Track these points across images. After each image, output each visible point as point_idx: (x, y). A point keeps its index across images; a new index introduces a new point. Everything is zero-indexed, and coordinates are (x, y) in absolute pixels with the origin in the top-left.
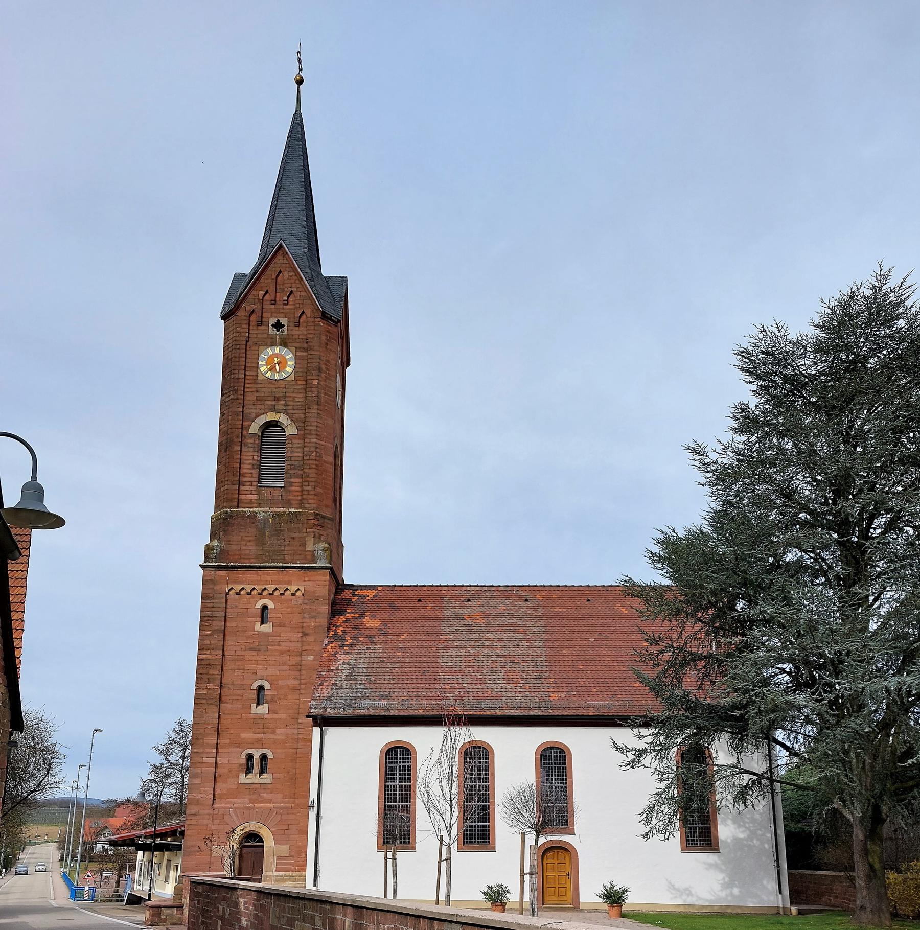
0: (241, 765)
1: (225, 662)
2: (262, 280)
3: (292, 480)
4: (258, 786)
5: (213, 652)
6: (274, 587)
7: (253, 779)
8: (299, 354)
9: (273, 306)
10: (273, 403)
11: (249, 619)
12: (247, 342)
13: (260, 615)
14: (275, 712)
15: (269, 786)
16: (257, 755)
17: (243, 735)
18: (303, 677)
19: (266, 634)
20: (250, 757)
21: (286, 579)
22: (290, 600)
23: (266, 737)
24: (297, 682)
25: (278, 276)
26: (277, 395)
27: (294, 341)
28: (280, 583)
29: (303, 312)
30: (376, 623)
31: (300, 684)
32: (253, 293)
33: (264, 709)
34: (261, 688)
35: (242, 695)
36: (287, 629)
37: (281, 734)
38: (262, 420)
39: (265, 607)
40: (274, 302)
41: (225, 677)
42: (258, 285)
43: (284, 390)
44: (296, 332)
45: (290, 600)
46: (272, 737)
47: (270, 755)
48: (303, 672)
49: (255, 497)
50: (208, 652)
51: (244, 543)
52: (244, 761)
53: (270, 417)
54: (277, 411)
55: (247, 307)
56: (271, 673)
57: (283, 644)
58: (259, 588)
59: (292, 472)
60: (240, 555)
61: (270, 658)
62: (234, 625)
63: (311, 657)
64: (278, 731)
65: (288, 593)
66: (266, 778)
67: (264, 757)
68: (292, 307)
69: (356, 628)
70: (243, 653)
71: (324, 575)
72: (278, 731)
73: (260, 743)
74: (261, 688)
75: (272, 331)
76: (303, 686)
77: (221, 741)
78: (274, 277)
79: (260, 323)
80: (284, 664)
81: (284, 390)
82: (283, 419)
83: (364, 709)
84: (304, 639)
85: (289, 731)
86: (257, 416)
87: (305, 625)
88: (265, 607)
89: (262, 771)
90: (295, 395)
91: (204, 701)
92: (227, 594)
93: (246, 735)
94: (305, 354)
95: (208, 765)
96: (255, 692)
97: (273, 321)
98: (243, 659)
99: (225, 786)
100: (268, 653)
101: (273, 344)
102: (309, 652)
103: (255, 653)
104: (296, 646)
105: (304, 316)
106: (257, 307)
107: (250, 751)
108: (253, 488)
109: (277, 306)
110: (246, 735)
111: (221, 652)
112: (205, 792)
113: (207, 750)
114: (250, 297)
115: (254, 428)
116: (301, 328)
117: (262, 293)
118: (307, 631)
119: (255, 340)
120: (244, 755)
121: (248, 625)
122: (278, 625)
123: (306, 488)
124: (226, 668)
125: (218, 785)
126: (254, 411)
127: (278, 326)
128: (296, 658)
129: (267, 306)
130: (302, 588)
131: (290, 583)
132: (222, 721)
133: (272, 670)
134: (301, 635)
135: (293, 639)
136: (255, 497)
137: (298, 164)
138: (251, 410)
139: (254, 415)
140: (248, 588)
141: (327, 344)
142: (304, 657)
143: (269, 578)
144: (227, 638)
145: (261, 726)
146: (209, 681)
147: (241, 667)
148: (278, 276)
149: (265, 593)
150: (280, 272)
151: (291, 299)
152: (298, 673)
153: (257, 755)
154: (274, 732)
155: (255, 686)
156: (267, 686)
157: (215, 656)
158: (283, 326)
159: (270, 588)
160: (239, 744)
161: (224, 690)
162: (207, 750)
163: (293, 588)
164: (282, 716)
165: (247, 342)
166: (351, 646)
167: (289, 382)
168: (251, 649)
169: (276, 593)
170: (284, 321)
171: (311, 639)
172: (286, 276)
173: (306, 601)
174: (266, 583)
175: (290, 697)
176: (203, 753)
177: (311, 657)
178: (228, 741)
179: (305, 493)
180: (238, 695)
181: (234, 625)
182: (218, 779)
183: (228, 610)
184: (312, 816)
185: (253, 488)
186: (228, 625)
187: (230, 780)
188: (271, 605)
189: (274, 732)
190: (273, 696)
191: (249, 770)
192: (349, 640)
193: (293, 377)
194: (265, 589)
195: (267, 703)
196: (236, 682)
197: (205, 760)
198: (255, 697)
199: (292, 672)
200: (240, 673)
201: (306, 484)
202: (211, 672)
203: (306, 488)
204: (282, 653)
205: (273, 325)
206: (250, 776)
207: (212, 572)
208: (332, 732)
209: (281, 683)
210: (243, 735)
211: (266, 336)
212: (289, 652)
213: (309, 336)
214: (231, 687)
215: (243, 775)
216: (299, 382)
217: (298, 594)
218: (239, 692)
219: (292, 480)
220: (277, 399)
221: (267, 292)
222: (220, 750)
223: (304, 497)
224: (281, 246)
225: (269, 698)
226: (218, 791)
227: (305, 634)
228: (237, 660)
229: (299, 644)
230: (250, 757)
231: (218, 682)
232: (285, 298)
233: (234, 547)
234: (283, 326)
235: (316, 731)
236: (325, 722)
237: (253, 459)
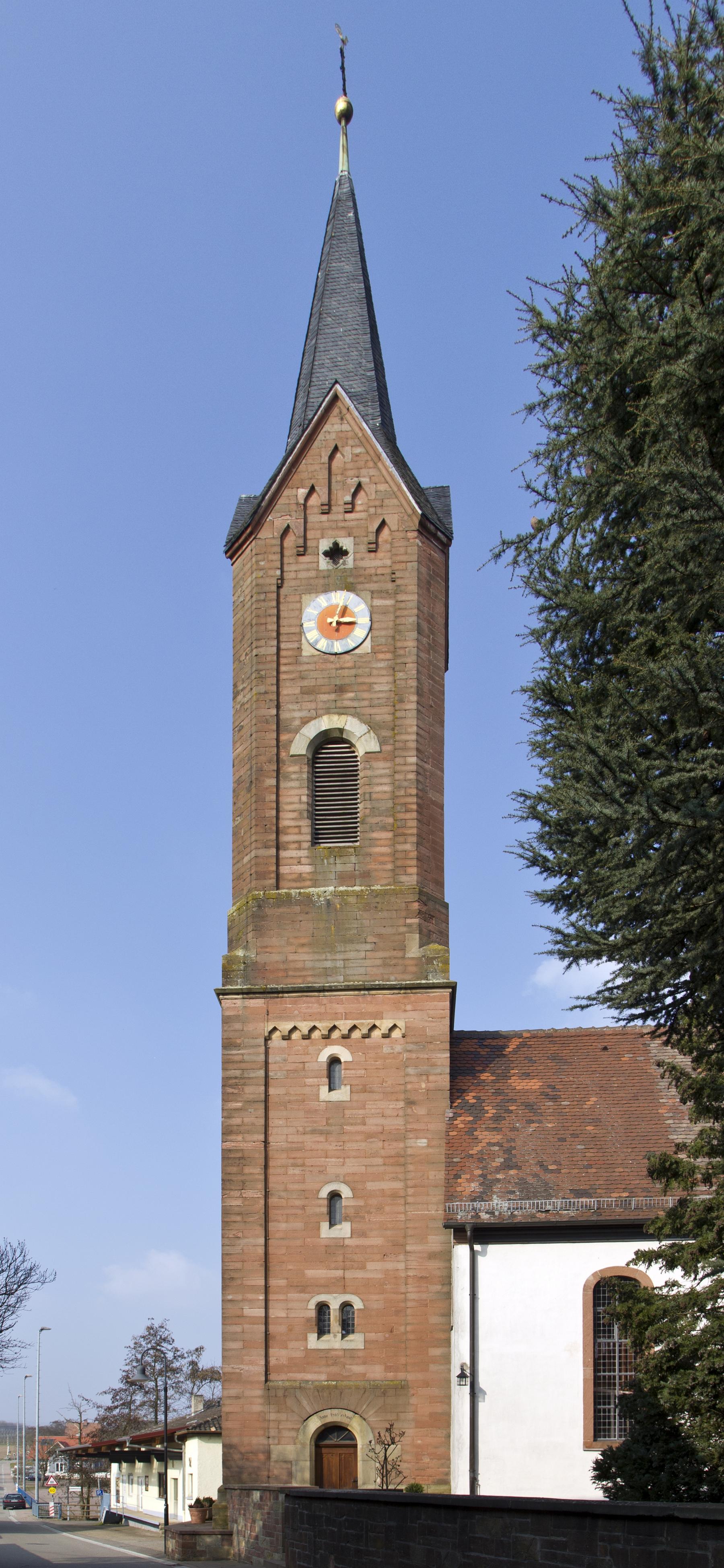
0: (308, 1320)
1: (271, 1154)
2: (302, 466)
3: (375, 835)
4: (341, 1353)
5: (248, 1137)
6: (350, 1023)
7: (333, 1341)
8: (378, 602)
9: (324, 518)
10: (333, 696)
11: (309, 1081)
12: (279, 587)
13: (325, 1072)
14: (363, 1234)
15: (360, 1354)
16: (334, 1303)
17: (311, 1273)
18: (410, 1176)
19: (339, 1106)
20: (322, 1308)
21: (371, 1008)
22: (380, 1047)
23: (349, 1274)
24: (398, 1185)
25: (331, 457)
26: (340, 681)
27: (369, 578)
28: (362, 1015)
29: (383, 524)
30: (535, 1084)
31: (407, 1187)
32: (287, 492)
33: (344, 1230)
34: (334, 1196)
35: (303, 1207)
36: (376, 1096)
37: (375, 1269)
38: (311, 731)
39: (334, 1061)
40: (327, 509)
41: (272, 1179)
42: (295, 478)
43: (353, 672)
44: (371, 563)
45: (380, 1047)
46: (360, 1274)
47: (358, 1304)
48: (411, 1167)
49: (307, 869)
50: (240, 1138)
51: (292, 949)
52: (313, 1314)
53: (326, 723)
54: (342, 711)
55: (276, 520)
56: (350, 1171)
57: (370, 1121)
58: (323, 1026)
59: (374, 820)
60: (286, 970)
61: (348, 1146)
62: (281, 1091)
63: (423, 1142)
64: (370, 1266)
65: (376, 1034)
66: (356, 1341)
67: (346, 1306)
68: (363, 515)
69: (498, 1092)
70: (300, 1138)
71: (440, 999)
72: (370, 1266)
73: (342, 1285)
74: (334, 1196)
75: (324, 563)
76: (410, 1191)
77: (273, 1282)
78: (325, 459)
79: (303, 550)
80: (374, 1155)
81: (353, 672)
82: (354, 727)
83: (559, 1207)
84: (409, 1111)
85: (390, 1265)
86: (305, 721)
87: (409, 1087)
88: (334, 1061)
89: (347, 1327)
90: (373, 680)
91: (238, 1218)
92: (267, 1039)
93: (314, 1273)
94: (389, 602)
95: (253, 1320)
96: (326, 1202)
97: (325, 545)
98: (298, 1149)
99: (284, 1352)
100: (346, 1138)
101: (326, 589)
102: (418, 1133)
103: (322, 1138)
104: (398, 1123)
105: (385, 532)
106: (294, 521)
107: (322, 1298)
108: (303, 853)
109: (332, 517)
110: (314, 1273)
111: (262, 1137)
112: (251, 1363)
113: (250, 1296)
114: (282, 501)
115: (300, 745)
116: (380, 554)
117: (302, 492)
118: (413, 1097)
119: (293, 583)
120: (312, 1305)
121: (307, 1090)
122: (361, 1089)
123: (400, 847)
124: (271, 1163)
125: (272, 1351)
126: (297, 714)
127: (336, 553)
128: (395, 1144)
129: (315, 518)
130: (401, 1024)
131: (379, 1015)
132: (271, 1250)
133: (353, 1166)
134: (401, 1104)
135: (388, 1112)
136: (307, 869)
137: (349, 267)
138: (291, 713)
139: (297, 723)
140: (305, 1027)
141: (429, 583)
142: (410, 1142)
143: (340, 1009)
144: (271, 1114)
145: (340, 1258)
146: (243, 1185)
147: (300, 1161)
148: (331, 457)
149: (336, 1035)
150: (336, 449)
151: (359, 501)
152: (399, 1169)
153: (334, 1303)
154: (363, 1267)
155: (324, 1193)
156: (346, 1192)
157: (252, 1143)
158: (346, 553)
159: (344, 1026)
160: (305, 1287)
161: (272, 1201)
162: (250, 1296)
163: (385, 1025)
164: (375, 1240)
165: (279, 587)
166: (497, 1118)
167: (361, 656)
168: (313, 1132)
169: (356, 1035)
170: (346, 543)
171: (420, 1111)
172: (348, 457)
173: (411, 1047)
174: (336, 1016)
175: (387, 1209)
176: (243, 1300)
177: (423, 1142)
178: (283, 1282)
179: (398, 855)
180: (297, 1207)
181: (281, 1091)
182: (271, 1343)
183: (271, 1067)
184: (461, 1396)
185: (303, 853)
186: (272, 1091)
187: (292, 1344)
188: (345, 1055)
189: (363, 1267)
190: (357, 1209)
191: (322, 1329)
192: (491, 1111)
193: (367, 647)
194: (334, 1027)
195: (346, 1218)
196: (291, 1187)
197: (248, 1311)
198: (325, 1210)
199: (390, 1169)
200: (297, 1171)
201: (401, 839)
202: (247, 1170)
203: (400, 847)
204: (369, 1136)
205: (326, 554)
206: (325, 1338)
207: (237, 1002)
208: (496, 1256)
209: (371, 1186)
210: (311, 1273)
211: (313, 574)
212: (383, 1135)
213: (397, 567)
214: (283, 1194)
215: (313, 1337)
216: (381, 656)
217: (396, 1034)
218: (298, 1203)
219: (375, 835)
220: (341, 689)
221: (312, 489)
222: (271, 1297)
223: (399, 863)
224: (336, 398)
225: (351, 1212)
226: (273, 1361)
227: (410, 1103)
228: (292, 1150)
229: (400, 1121)
230: (322, 1308)
231: (261, 1185)
232: (348, 498)
233: (276, 957)
234: (346, 553)
235: (462, 1252)
236: (485, 1234)
237: (300, 802)
